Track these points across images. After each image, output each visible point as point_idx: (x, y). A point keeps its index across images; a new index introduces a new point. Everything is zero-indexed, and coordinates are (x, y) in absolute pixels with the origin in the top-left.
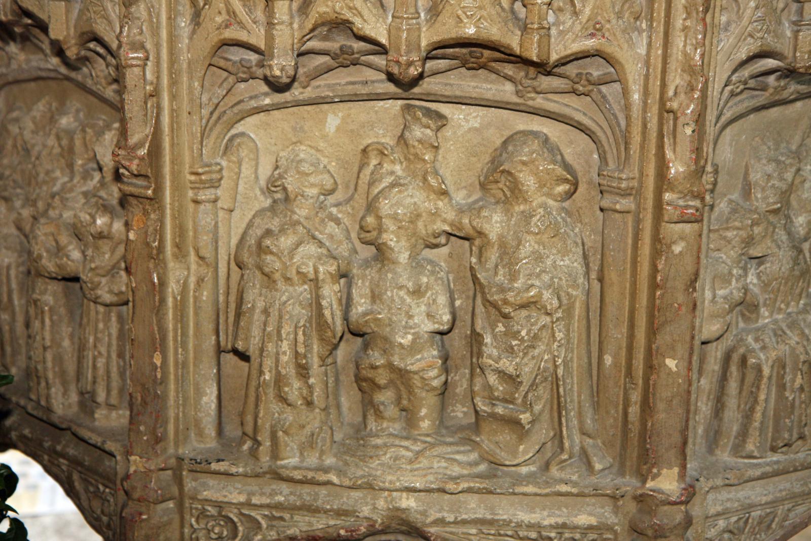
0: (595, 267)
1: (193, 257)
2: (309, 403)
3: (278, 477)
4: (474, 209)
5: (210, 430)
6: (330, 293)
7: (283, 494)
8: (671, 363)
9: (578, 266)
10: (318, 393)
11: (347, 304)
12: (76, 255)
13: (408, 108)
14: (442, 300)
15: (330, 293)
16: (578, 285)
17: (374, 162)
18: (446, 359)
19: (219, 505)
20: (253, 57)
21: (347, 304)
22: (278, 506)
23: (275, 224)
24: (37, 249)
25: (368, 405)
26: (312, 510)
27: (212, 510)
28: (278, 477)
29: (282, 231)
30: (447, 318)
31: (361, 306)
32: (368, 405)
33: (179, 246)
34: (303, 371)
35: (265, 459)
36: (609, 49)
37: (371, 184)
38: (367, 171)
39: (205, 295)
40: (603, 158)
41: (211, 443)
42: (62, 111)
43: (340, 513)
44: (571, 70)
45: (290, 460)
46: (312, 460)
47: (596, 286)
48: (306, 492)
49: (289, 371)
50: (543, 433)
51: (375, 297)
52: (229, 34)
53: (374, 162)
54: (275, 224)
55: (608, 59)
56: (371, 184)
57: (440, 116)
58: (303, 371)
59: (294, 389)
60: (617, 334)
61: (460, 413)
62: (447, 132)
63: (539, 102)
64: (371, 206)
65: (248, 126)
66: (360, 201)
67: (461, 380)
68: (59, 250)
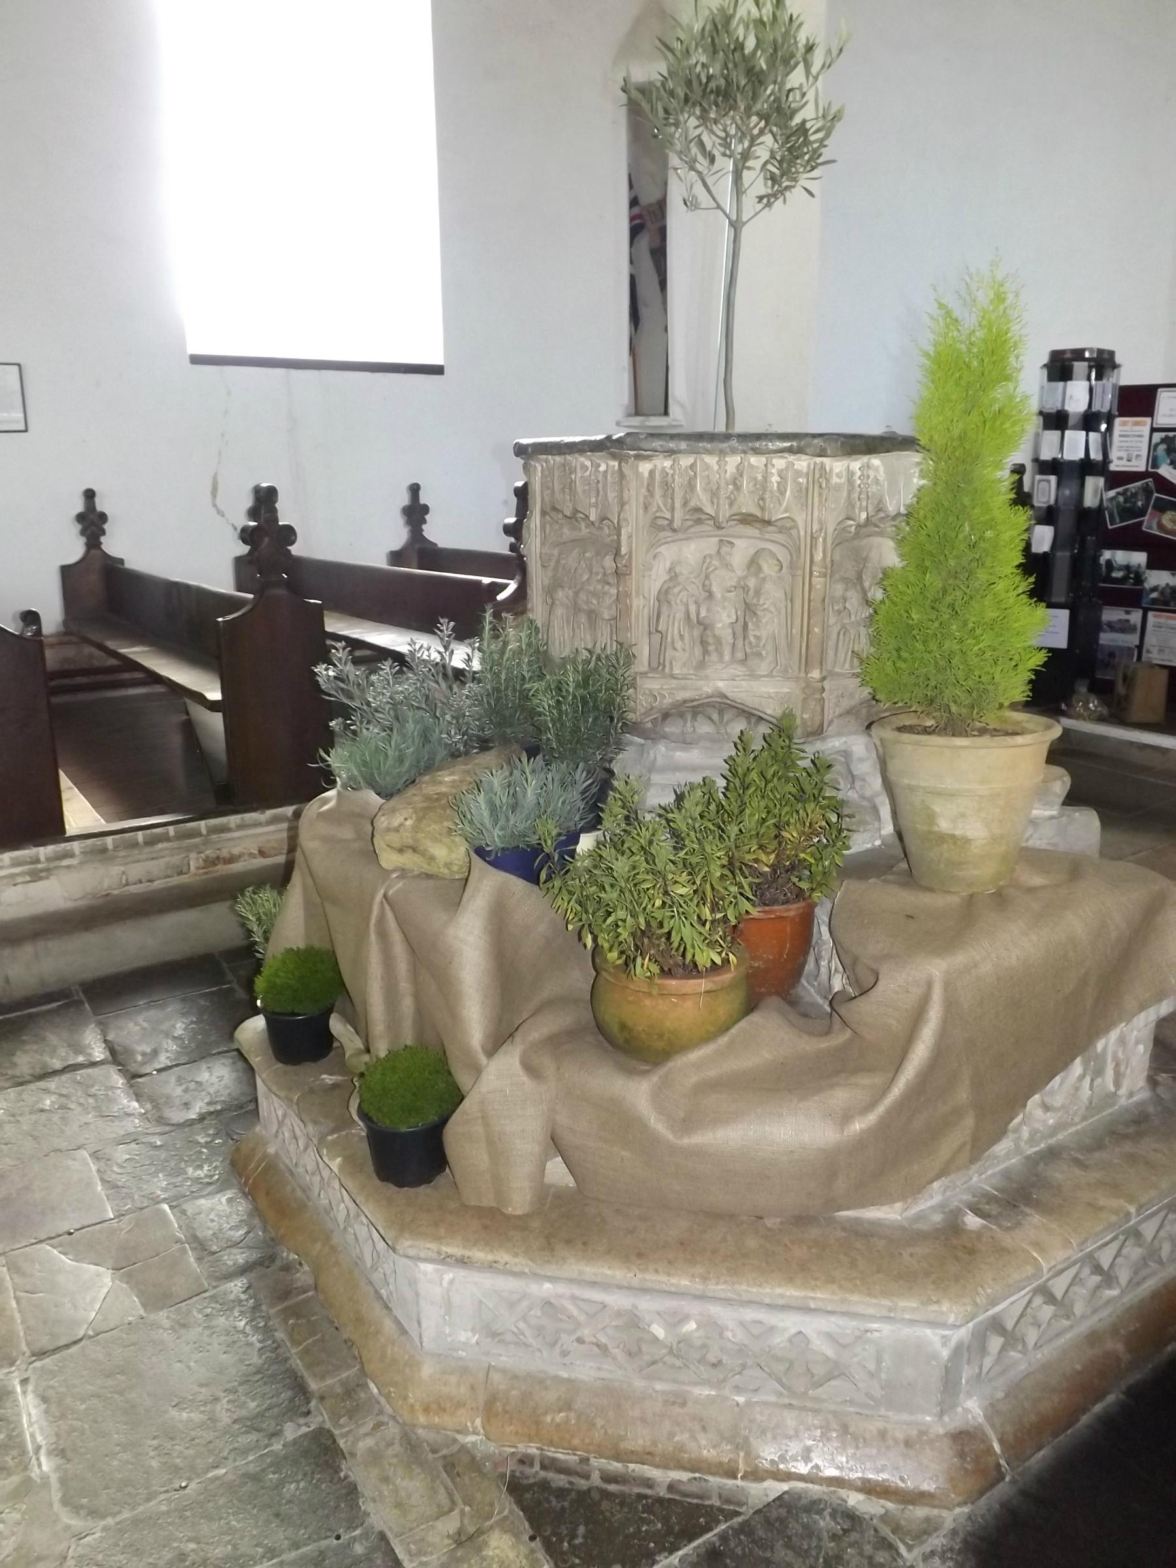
0: (789, 597)
1: (641, 597)
2: (684, 650)
3: (673, 677)
4: (745, 578)
5: (646, 664)
6: (693, 608)
7: (674, 683)
8: (816, 630)
9: (783, 597)
10: (687, 647)
11: (698, 614)
12: (595, 602)
13: (721, 541)
14: (733, 611)
15: (693, 608)
16: (951, 1182)
17: (708, 561)
18: (734, 634)
19: (650, 691)
20: (666, 522)
21: (698, 614)
22: (672, 689)
23: (671, 584)
24: (579, 602)
25: (706, 652)
26: (684, 688)
27: (647, 692)
28: (673, 677)
29: (675, 587)
30: (735, 617)
31: (703, 614)
32: (706, 652)
33: (637, 592)
34: (682, 637)
35: (667, 670)
36: (793, 516)
37: (707, 569)
38: (705, 565)
39: (646, 611)
40: (791, 555)
41: (646, 669)
42: (585, 552)
43: (697, 689)
44: (778, 523)
45: (676, 671)
46: (685, 671)
47: (789, 604)
48: (683, 682)
49: (677, 637)
50: (770, 658)
51: (708, 610)
52: (658, 514)
53: (708, 561)
54: (671, 584)
55: (793, 520)
56: (707, 569)
57: (732, 543)
58: (682, 637)
59: (679, 645)
60: (798, 621)
61: (740, 655)
62: (735, 549)
63: (767, 536)
64: (707, 577)
65: (662, 549)
66: (703, 576)
67: (740, 643)
68: (587, 602)
